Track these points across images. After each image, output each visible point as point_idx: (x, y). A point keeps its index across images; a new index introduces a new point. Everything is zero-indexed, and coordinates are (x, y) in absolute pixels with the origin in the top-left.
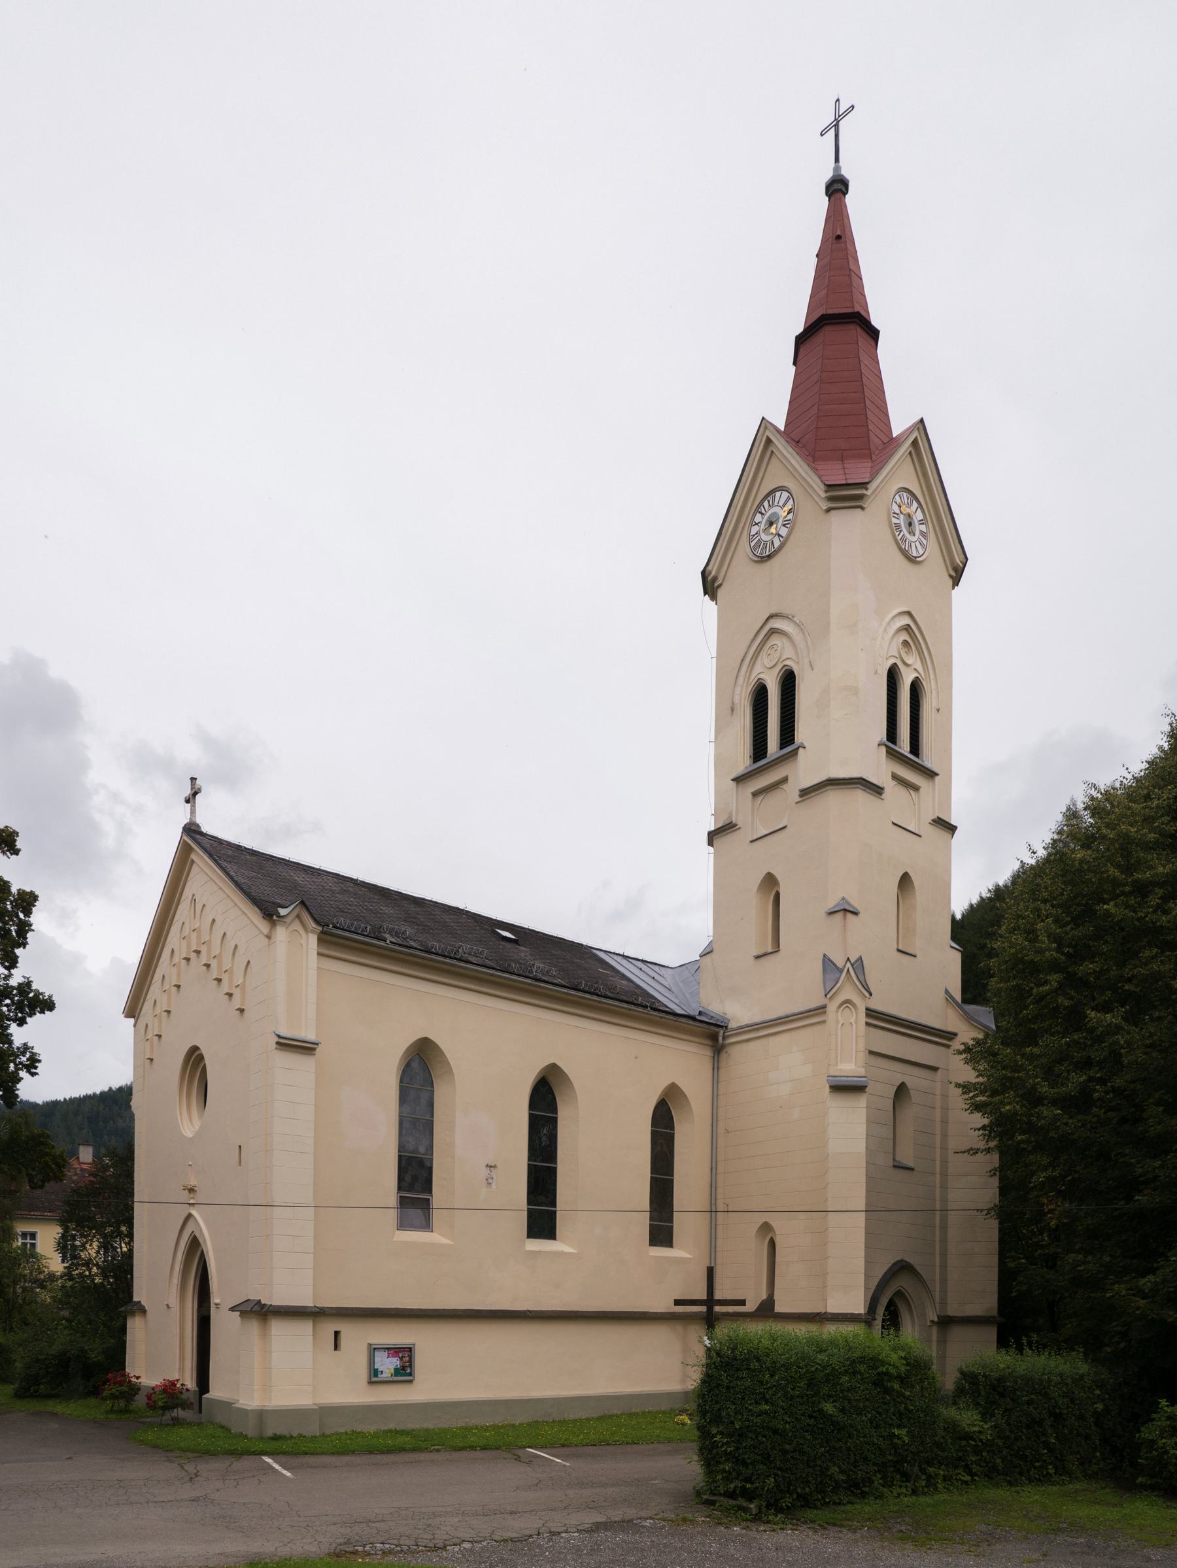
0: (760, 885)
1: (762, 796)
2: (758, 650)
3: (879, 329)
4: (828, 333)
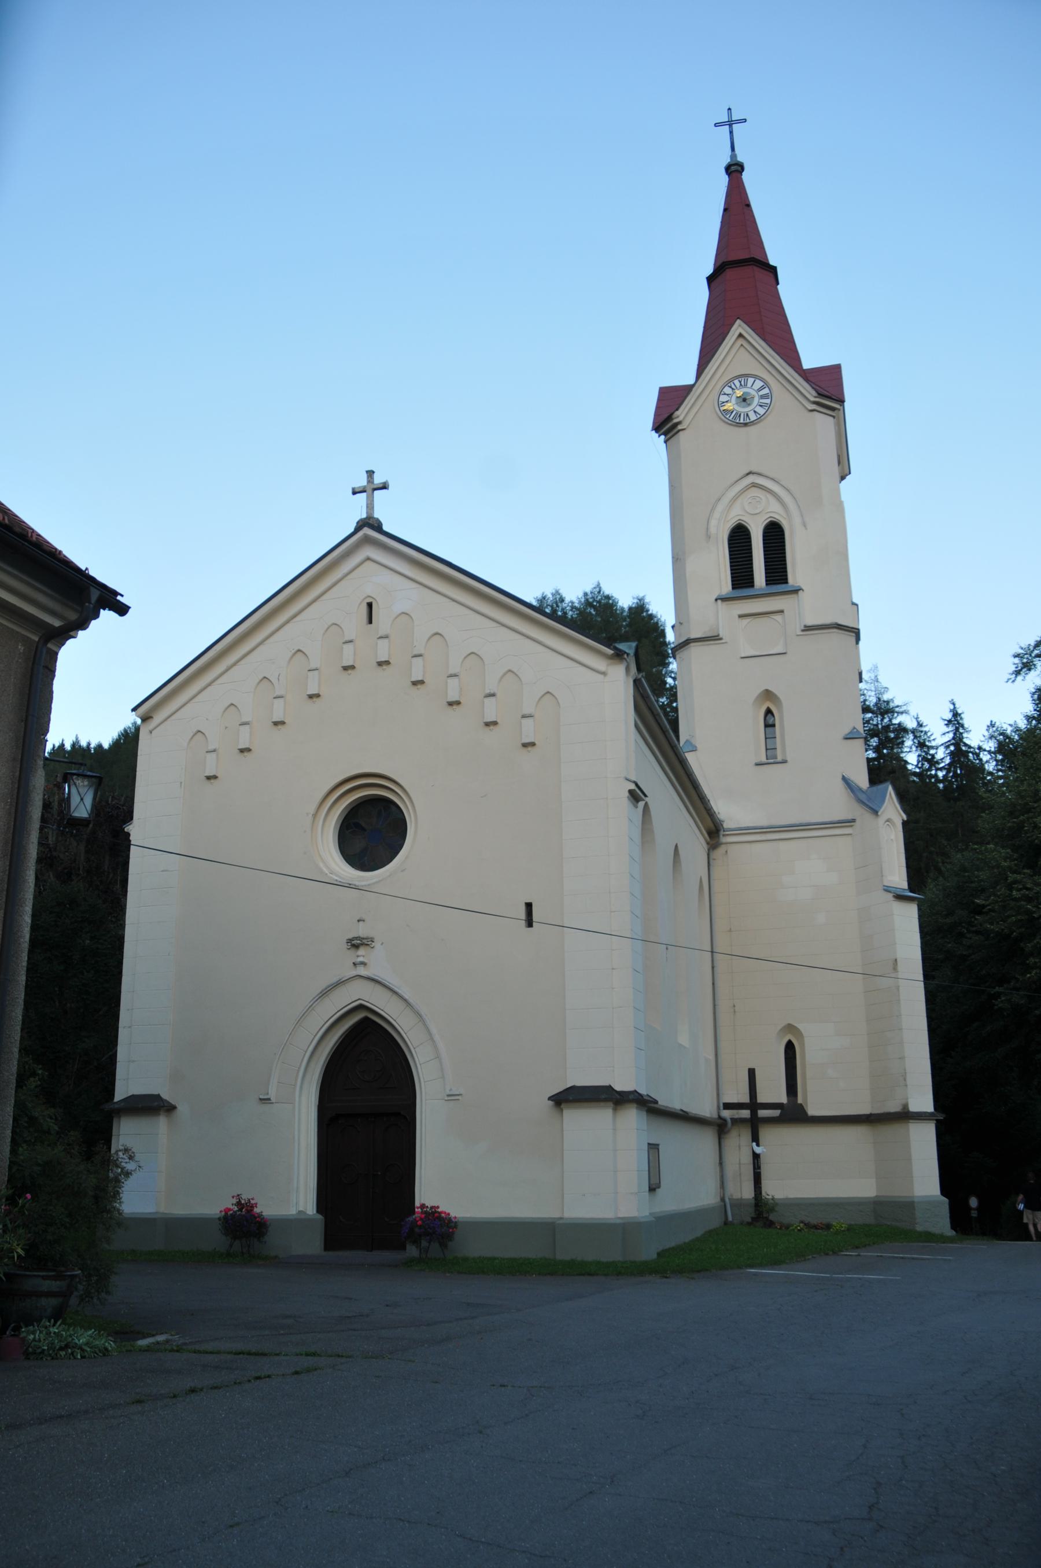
0: (757, 697)
1: (750, 619)
2: (736, 497)
3: (775, 265)
4: (729, 274)
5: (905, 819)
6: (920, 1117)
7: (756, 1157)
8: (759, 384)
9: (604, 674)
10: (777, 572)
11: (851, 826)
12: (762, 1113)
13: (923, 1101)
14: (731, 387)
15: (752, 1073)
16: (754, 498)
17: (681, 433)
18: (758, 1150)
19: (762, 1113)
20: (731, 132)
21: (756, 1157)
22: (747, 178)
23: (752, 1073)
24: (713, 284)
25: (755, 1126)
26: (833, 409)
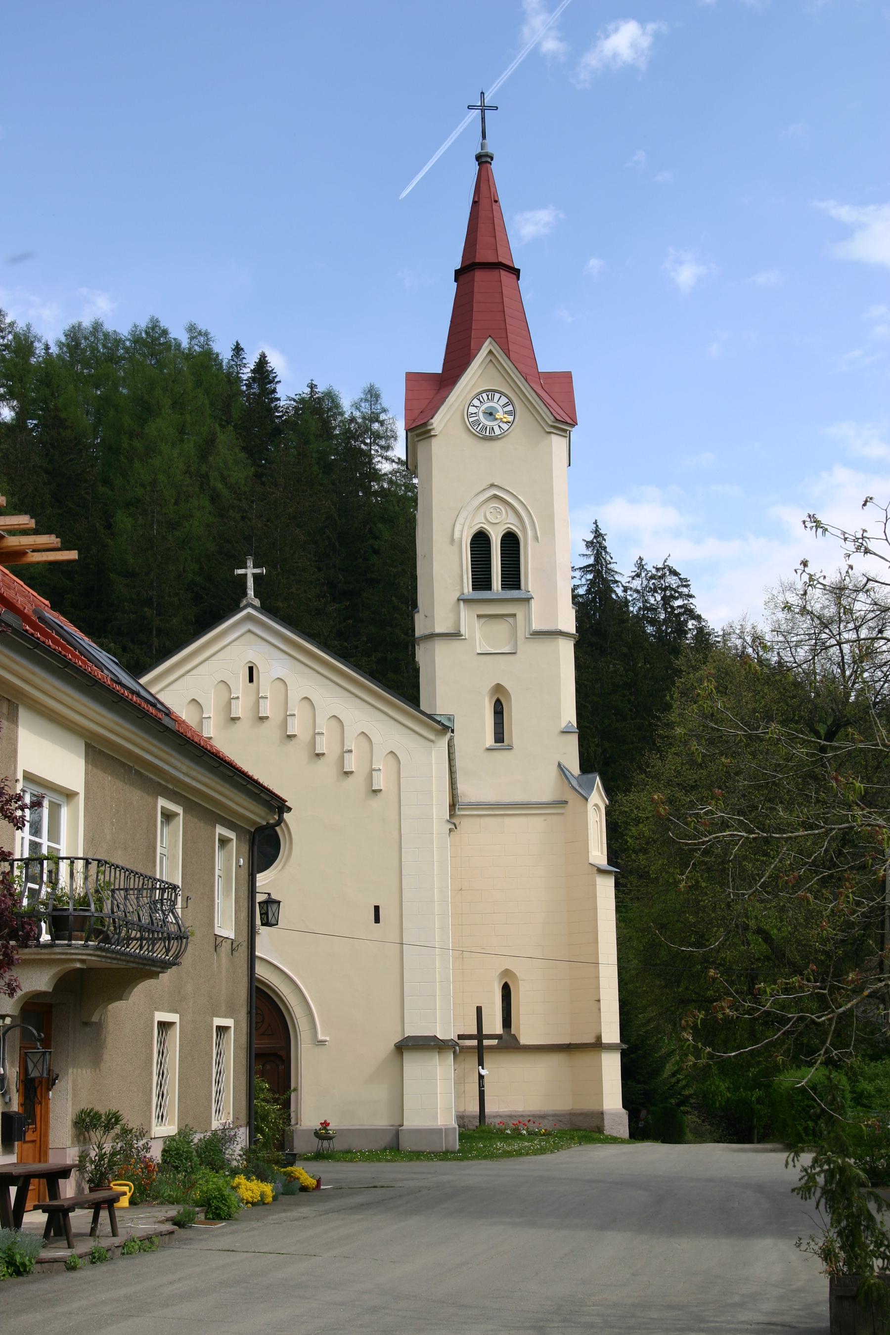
5: (608, 803)
6: (610, 1047)
7: (481, 1077)
8: (504, 400)
9: (432, 741)
10: (512, 579)
11: (564, 807)
12: (486, 1042)
13: (611, 1033)
14: (479, 400)
15: (479, 1010)
16: (495, 508)
17: (433, 438)
18: (483, 1072)
19: (486, 1042)
20: (483, 119)
21: (481, 1077)
22: (496, 168)
23: (479, 1010)
24: (461, 278)
25: (480, 1053)
26: (565, 431)
